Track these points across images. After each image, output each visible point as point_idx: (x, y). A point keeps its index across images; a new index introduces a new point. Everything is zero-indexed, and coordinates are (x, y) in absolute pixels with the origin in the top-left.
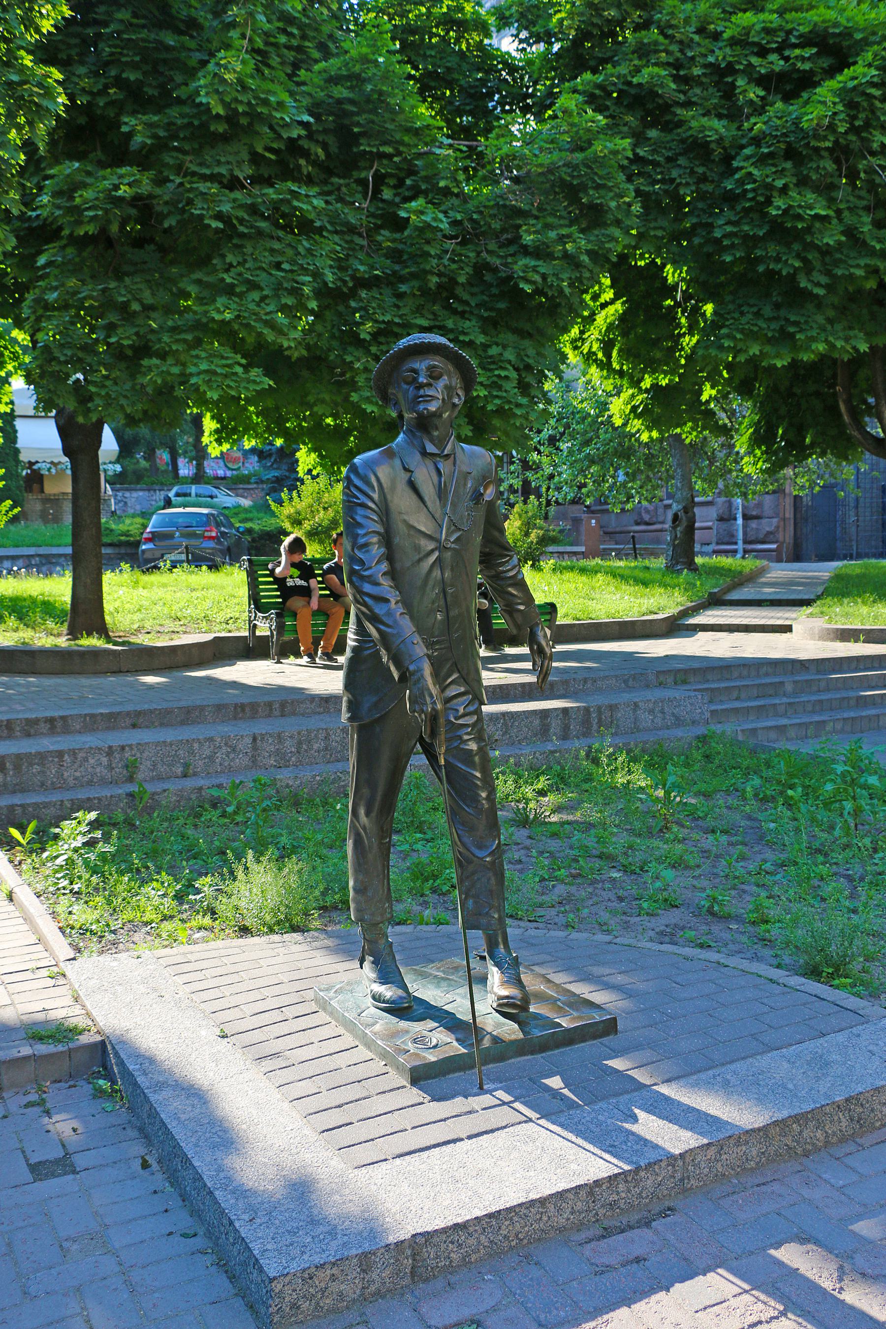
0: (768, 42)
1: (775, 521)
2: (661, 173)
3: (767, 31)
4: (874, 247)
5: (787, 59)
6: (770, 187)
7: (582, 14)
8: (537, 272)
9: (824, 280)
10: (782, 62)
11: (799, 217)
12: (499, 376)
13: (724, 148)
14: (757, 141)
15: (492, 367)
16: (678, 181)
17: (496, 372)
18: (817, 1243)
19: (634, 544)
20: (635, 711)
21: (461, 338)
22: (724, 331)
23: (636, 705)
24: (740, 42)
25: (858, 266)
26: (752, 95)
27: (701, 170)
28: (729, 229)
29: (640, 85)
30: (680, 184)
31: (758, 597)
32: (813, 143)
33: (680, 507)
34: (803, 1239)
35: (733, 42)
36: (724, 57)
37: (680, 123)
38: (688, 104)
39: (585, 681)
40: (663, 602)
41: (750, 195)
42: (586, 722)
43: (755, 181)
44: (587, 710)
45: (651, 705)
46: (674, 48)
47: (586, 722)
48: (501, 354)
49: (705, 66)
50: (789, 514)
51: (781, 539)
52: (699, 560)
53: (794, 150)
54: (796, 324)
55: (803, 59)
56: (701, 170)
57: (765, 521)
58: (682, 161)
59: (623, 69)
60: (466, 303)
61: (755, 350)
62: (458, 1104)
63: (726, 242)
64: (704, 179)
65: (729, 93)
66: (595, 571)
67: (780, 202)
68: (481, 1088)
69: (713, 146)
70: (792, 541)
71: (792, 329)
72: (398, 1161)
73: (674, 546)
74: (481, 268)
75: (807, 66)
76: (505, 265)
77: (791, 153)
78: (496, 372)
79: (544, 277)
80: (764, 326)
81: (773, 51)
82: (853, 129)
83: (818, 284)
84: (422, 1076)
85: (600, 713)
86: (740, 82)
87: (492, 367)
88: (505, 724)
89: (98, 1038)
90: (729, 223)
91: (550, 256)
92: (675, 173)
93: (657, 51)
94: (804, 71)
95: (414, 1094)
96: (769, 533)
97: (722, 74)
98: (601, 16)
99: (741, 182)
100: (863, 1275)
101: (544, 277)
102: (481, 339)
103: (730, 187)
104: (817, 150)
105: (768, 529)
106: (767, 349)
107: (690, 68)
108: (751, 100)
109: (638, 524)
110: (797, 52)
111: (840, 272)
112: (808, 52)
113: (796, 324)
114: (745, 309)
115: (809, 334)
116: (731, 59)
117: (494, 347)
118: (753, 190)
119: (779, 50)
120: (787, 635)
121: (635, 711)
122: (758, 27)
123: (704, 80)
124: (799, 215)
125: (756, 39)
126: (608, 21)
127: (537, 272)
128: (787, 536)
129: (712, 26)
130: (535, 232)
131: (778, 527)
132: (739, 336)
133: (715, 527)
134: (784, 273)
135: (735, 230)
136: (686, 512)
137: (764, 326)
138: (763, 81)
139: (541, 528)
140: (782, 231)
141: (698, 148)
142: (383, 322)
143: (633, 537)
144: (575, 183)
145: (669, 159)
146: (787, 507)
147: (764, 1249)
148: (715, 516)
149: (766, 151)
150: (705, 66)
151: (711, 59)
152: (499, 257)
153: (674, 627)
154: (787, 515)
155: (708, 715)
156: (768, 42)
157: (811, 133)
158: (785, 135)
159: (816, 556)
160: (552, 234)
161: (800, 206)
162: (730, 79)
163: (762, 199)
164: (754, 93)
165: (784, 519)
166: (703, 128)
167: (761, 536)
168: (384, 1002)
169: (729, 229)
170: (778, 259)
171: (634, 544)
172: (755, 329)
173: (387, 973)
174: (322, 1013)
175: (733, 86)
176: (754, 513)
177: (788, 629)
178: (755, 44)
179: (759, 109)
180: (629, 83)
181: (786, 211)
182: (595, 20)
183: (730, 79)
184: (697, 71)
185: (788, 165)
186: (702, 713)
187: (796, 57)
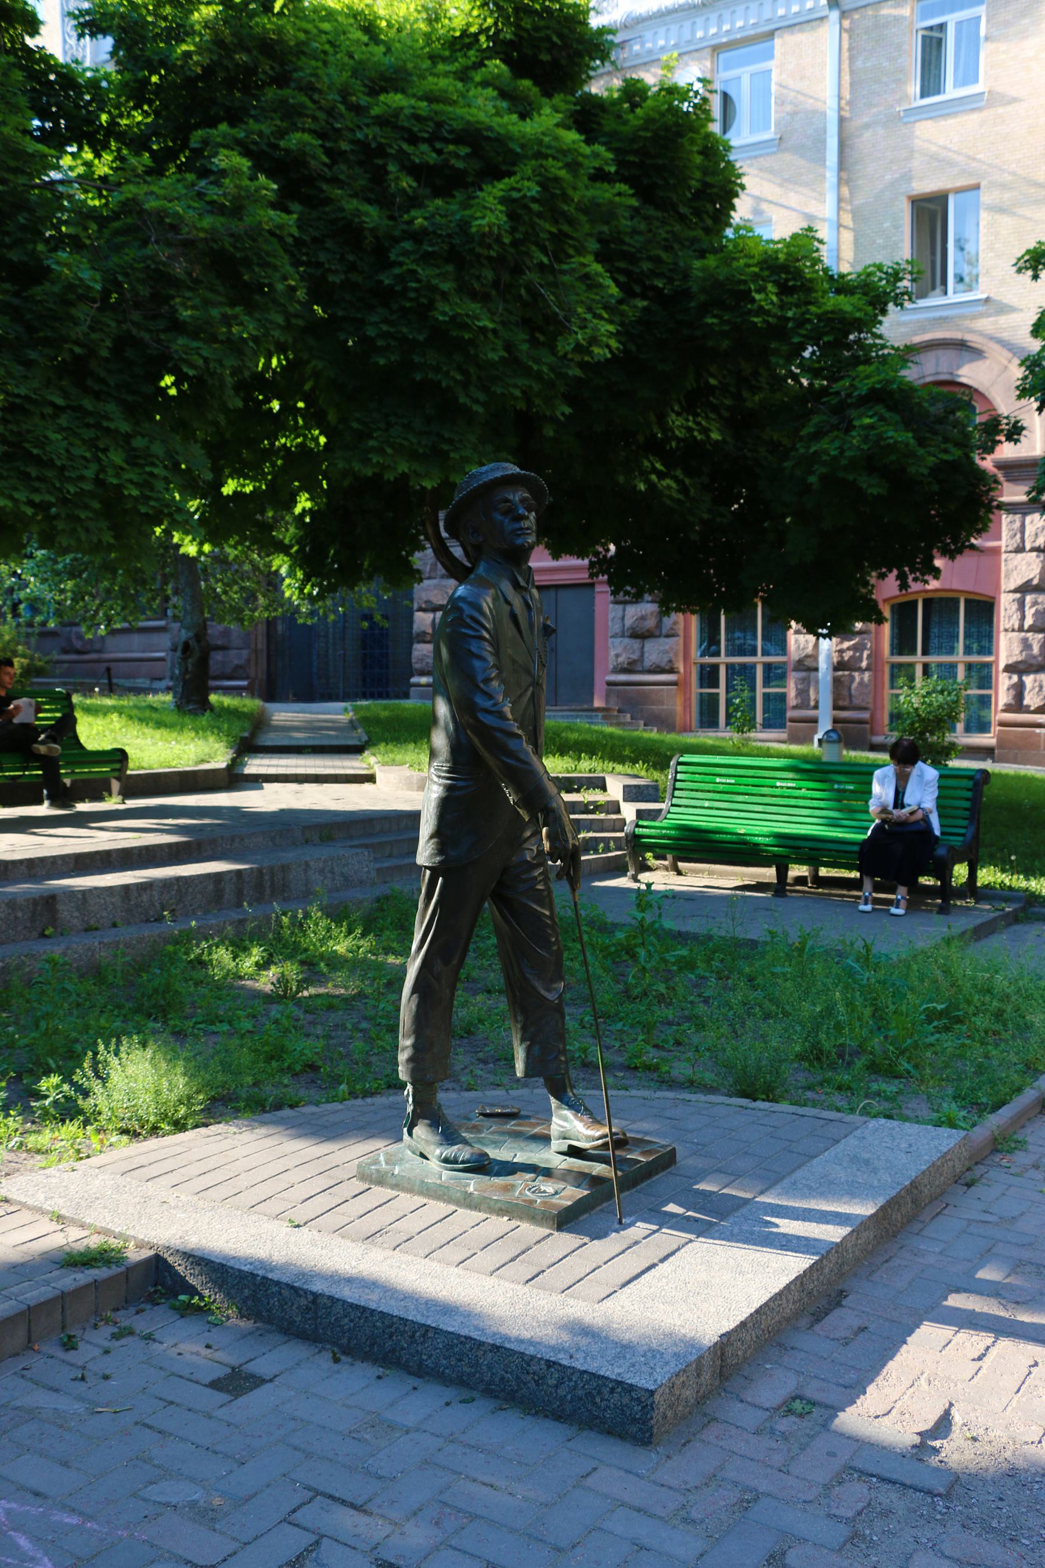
0: (420, 131)
1: (245, 653)
2: (307, 254)
3: (417, 118)
4: (531, 368)
5: (439, 152)
6: (434, 289)
7: (209, 50)
8: (200, 355)
9: (482, 397)
10: (434, 155)
11: (465, 326)
12: (151, 474)
13: (376, 237)
14: (418, 237)
15: (142, 462)
16: (327, 266)
17: (148, 469)
18: (965, 1291)
19: (110, 679)
20: (306, 871)
21: (105, 424)
22: (372, 443)
23: (307, 864)
24: (386, 121)
25: (515, 386)
26: (405, 184)
27: (351, 258)
28: (385, 328)
29: (286, 150)
30: (330, 270)
31: (286, 742)
32: (478, 250)
33: (190, 634)
34: (958, 1291)
35: (382, 121)
36: (374, 138)
37: (328, 201)
38: (335, 181)
39: (233, 839)
40: (211, 752)
41: (412, 295)
42: (259, 887)
43: (418, 281)
44: (260, 871)
45: (321, 865)
46: (321, 115)
47: (259, 887)
48: (148, 448)
49: (353, 142)
50: (262, 644)
51: (252, 674)
52: (213, 698)
53: (459, 251)
54: (450, 441)
55: (457, 156)
56: (351, 258)
57: (232, 653)
58: (329, 244)
59: (266, 128)
60: (103, 381)
61: (403, 467)
62: (613, 1243)
63: (380, 343)
64: (352, 268)
65: (379, 176)
66: (105, 711)
67: (442, 306)
68: (620, 1222)
69: (367, 233)
70: (265, 677)
71: (446, 447)
72: (625, 1289)
73: (185, 682)
74: (122, 342)
75: (460, 165)
76: (159, 341)
77: (454, 256)
78: (148, 469)
79: (206, 360)
80: (414, 440)
81: (424, 140)
82: (514, 243)
83: (476, 401)
84: (566, 1220)
85: (272, 875)
86: (392, 168)
87: (142, 462)
88: (179, 891)
89: (152, 1253)
90: (386, 321)
91: (213, 339)
92: (322, 257)
93: (301, 115)
94: (459, 169)
95: (566, 1240)
96: (238, 667)
97: (370, 155)
98: (233, 59)
99: (401, 279)
100: (1017, 1303)
101: (206, 360)
102: (125, 427)
103: (387, 282)
104: (478, 256)
105: (236, 662)
106: (416, 466)
107: (335, 141)
108: (404, 190)
109: (66, 652)
110: (451, 147)
111: (499, 391)
112: (464, 150)
113: (450, 441)
114: (393, 419)
115: (463, 454)
116: (383, 141)
117: (139, 438)
118: (416, 290)
119: (429, 141)
120: (367, 786)
121: (306, 871)
122: (407, 111)
123: (352, 157)
124: (466, 324)
125: (406, 124)
126: (238, 65)
127: (200, 355)
128: (259, 670)
129: (354, 98)
130: (193, 308)
131: (249, 661)
132: (389, 451)
133: (169, 659)
134: (444, 384)
135: (392, 330)
136: (198, 641)
137: (414, 440)
138: (415, 170)
139: (24, 656)
140: (449, 340)
141: (349, 232)
142: (18, 396)
143: (108, 670)
144: (238, 255)
145: (315, 240)
146: (260, 637)
147: (939, 1304)
148: (169, 644)
149: (430, 249)
150: (353, 142)
151: (359, 135)
152: (148, 330)
153: (232, 779)
154: (259, 646)
155: (374, 874)
156: (420, 131)
157: (477, 239)
158: (449, 236)
159: (295, 695)
160: (215, 312)
161: (467, 315)
162: (380, 162)
163: (425, 301)
164: (407, 183)
165: (256, 651)
166: (358, 213)
167: (228, 670)
168: (463, 1162)
169: (385, 328)
170: (437, 369)
171: (110, 679)
172: (406, 444)
173: (450, 1137)
174: (376, 1189)
175: (384, 167)
176: (219, 643)
177: (370, 779)
178: (403, 128)
179: (414, 202)
180: (275, 147)
181: (453, 318)
182: (225, 62)
183: (380, 162)
184: (344, 146)
185: (450, 268)
186: (368, 872)
187: (450, 153)
